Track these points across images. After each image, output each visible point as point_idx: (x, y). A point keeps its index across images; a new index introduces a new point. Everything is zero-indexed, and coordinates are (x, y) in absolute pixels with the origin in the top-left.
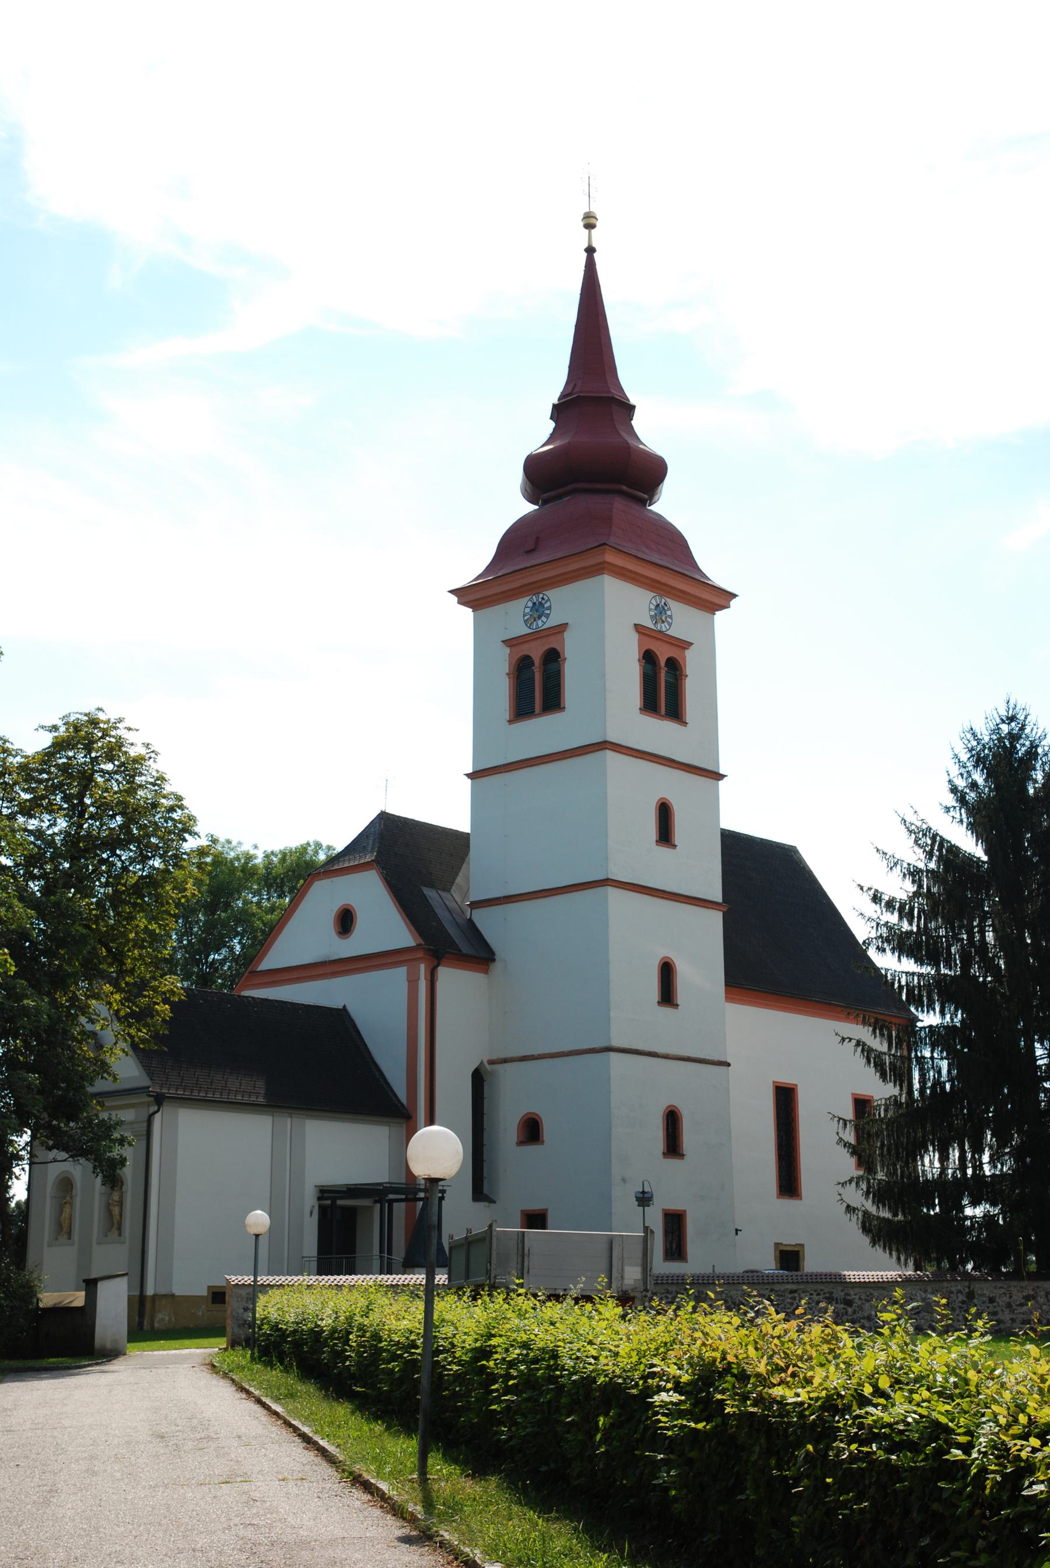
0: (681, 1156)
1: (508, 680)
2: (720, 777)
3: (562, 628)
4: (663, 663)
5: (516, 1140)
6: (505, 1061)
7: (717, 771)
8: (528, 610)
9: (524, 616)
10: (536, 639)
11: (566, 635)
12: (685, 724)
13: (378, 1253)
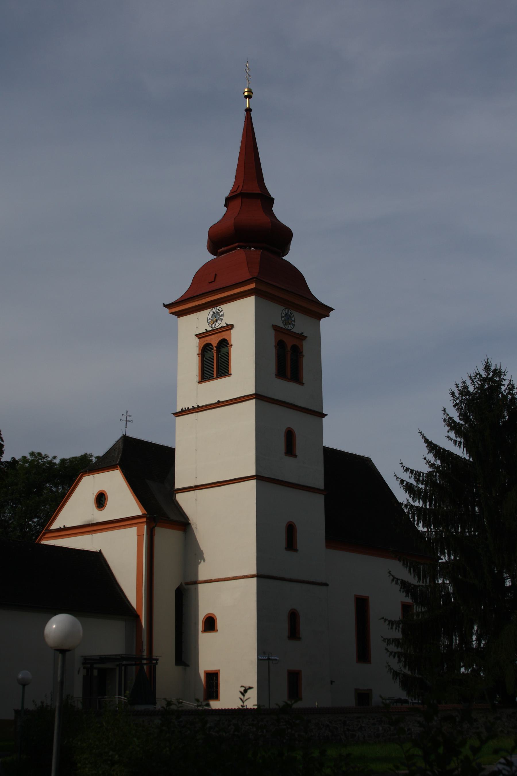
0: (299, 639)
2: (325, 415)
3: (230, 327)
4: (289, 348)
7: (321, 412)
8: (210, 317)
9: (208, 320)
11: (232, 331)
12: (302, 384)
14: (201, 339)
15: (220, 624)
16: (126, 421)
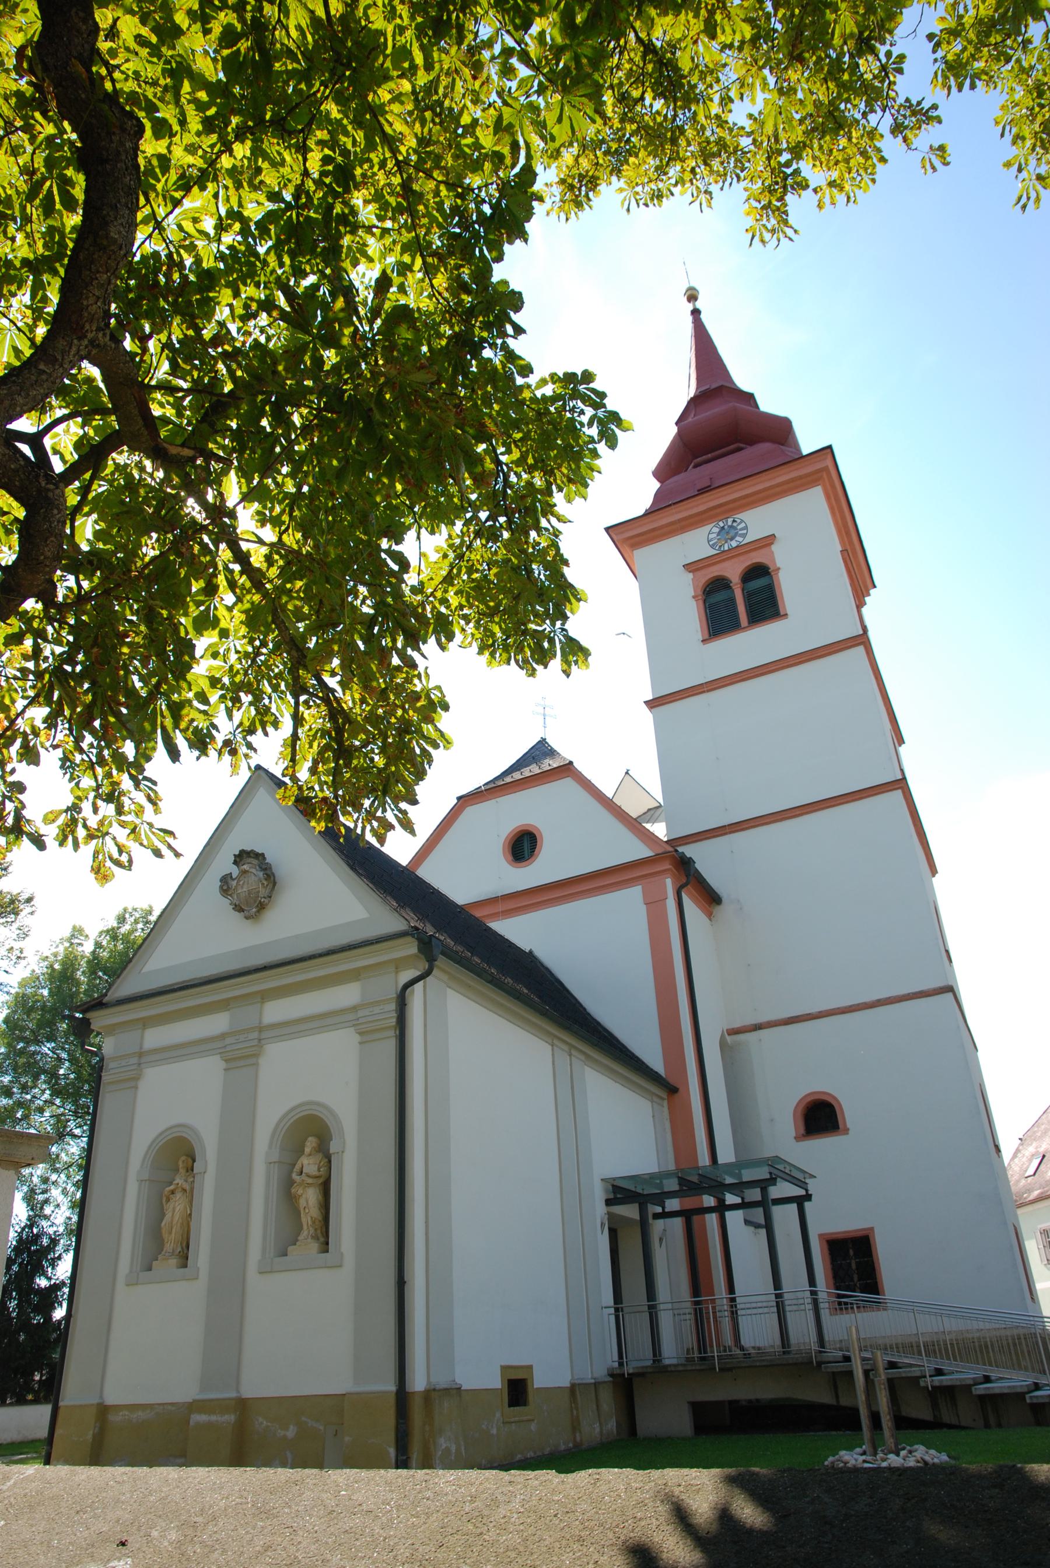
1: (694, 603)
5: (794, 1134)
6: (758, 1027)
10: (732, 557)
11: (774, 548)
13: (611, 1302)
14: (698, 573)
15: (850, 1112)
16: (544, 715)
